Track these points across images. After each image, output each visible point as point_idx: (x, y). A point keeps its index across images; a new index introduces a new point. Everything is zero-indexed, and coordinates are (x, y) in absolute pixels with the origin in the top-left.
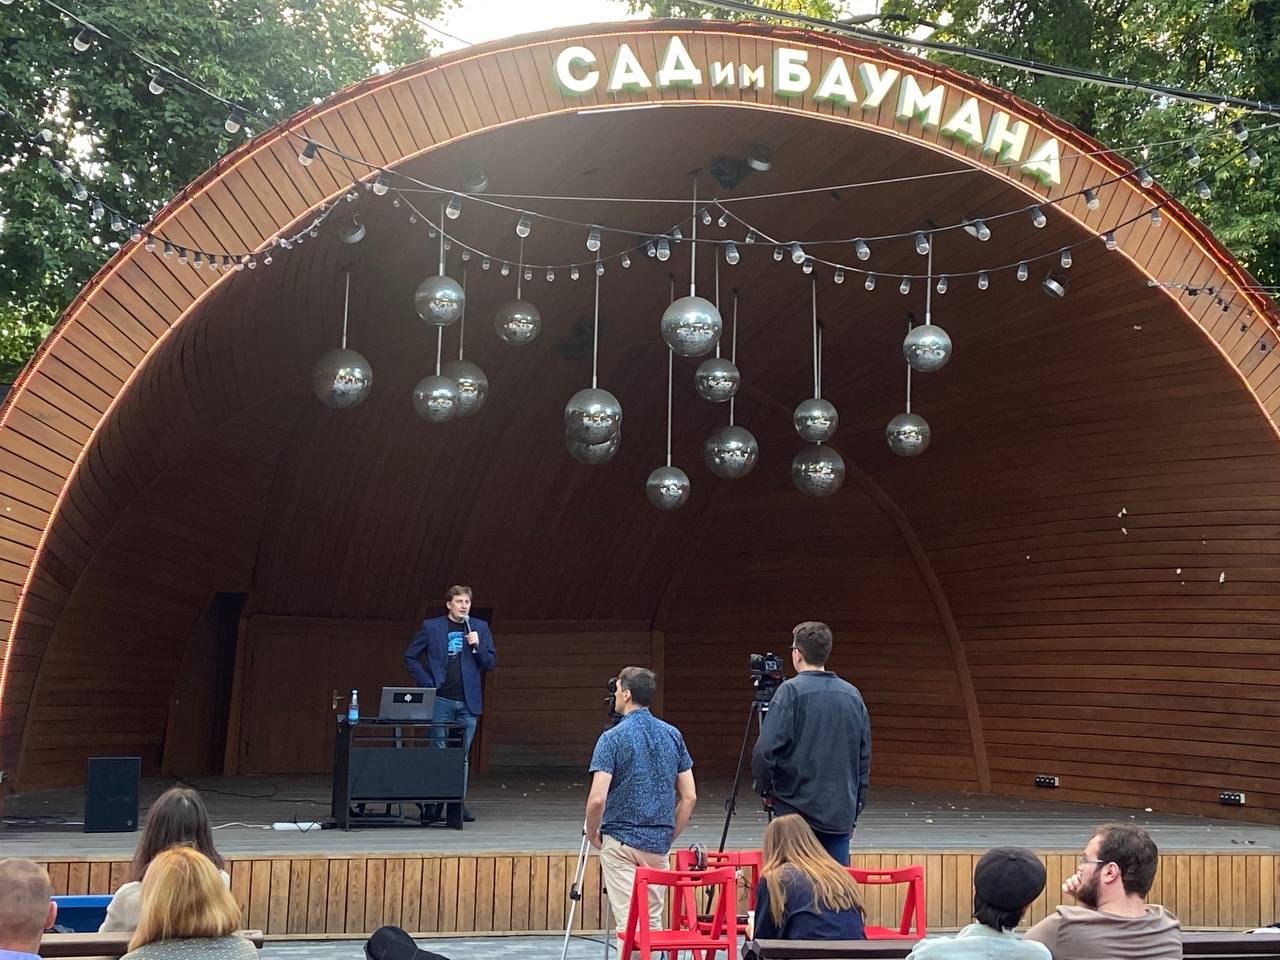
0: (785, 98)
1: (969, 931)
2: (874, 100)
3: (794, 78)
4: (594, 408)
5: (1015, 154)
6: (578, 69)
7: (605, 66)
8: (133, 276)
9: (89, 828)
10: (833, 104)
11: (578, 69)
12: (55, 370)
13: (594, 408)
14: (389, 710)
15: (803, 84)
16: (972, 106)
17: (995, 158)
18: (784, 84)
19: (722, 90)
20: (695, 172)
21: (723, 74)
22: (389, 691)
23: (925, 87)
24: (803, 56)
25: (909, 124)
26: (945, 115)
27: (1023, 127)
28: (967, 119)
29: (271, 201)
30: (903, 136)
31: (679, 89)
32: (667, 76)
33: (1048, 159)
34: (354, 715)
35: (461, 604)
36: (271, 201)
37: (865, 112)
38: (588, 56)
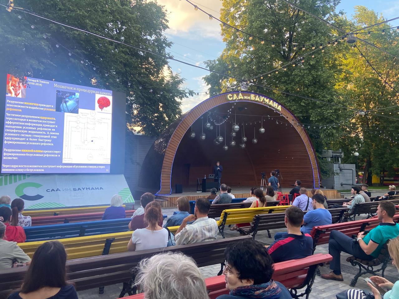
0: (252, 100)
1: (283, 288)
2: (261, 101)
3: (253, 98)
4: (236, 127)
5: (276, 107)
6: (230, 97)
7: (233, 97)
8: (177, 132)
9: (176, 193)
10: (257, 101)
11: (230, 97)
12: (172, 140)
13: (236, 127)
14: (210, 177)
15: (254, 99)
16: (272, 101)
17: (274, 108)
18: (252, 99)
19: (245, 100)
21: (246, 97)
22: (210, 175)
23: (267, 99)
24: (254, 95)
25: (265, 104)
26: (269, 102)
27: (277, 104)
28: (257, 99)
29: (173, 146)
31: (241, 99)
32: (240, 98)
33: (279, 108)
34: (205, 178)
35: (218, 164)
36: (173, 146)
37: (260, 102)
38: (231, 96)
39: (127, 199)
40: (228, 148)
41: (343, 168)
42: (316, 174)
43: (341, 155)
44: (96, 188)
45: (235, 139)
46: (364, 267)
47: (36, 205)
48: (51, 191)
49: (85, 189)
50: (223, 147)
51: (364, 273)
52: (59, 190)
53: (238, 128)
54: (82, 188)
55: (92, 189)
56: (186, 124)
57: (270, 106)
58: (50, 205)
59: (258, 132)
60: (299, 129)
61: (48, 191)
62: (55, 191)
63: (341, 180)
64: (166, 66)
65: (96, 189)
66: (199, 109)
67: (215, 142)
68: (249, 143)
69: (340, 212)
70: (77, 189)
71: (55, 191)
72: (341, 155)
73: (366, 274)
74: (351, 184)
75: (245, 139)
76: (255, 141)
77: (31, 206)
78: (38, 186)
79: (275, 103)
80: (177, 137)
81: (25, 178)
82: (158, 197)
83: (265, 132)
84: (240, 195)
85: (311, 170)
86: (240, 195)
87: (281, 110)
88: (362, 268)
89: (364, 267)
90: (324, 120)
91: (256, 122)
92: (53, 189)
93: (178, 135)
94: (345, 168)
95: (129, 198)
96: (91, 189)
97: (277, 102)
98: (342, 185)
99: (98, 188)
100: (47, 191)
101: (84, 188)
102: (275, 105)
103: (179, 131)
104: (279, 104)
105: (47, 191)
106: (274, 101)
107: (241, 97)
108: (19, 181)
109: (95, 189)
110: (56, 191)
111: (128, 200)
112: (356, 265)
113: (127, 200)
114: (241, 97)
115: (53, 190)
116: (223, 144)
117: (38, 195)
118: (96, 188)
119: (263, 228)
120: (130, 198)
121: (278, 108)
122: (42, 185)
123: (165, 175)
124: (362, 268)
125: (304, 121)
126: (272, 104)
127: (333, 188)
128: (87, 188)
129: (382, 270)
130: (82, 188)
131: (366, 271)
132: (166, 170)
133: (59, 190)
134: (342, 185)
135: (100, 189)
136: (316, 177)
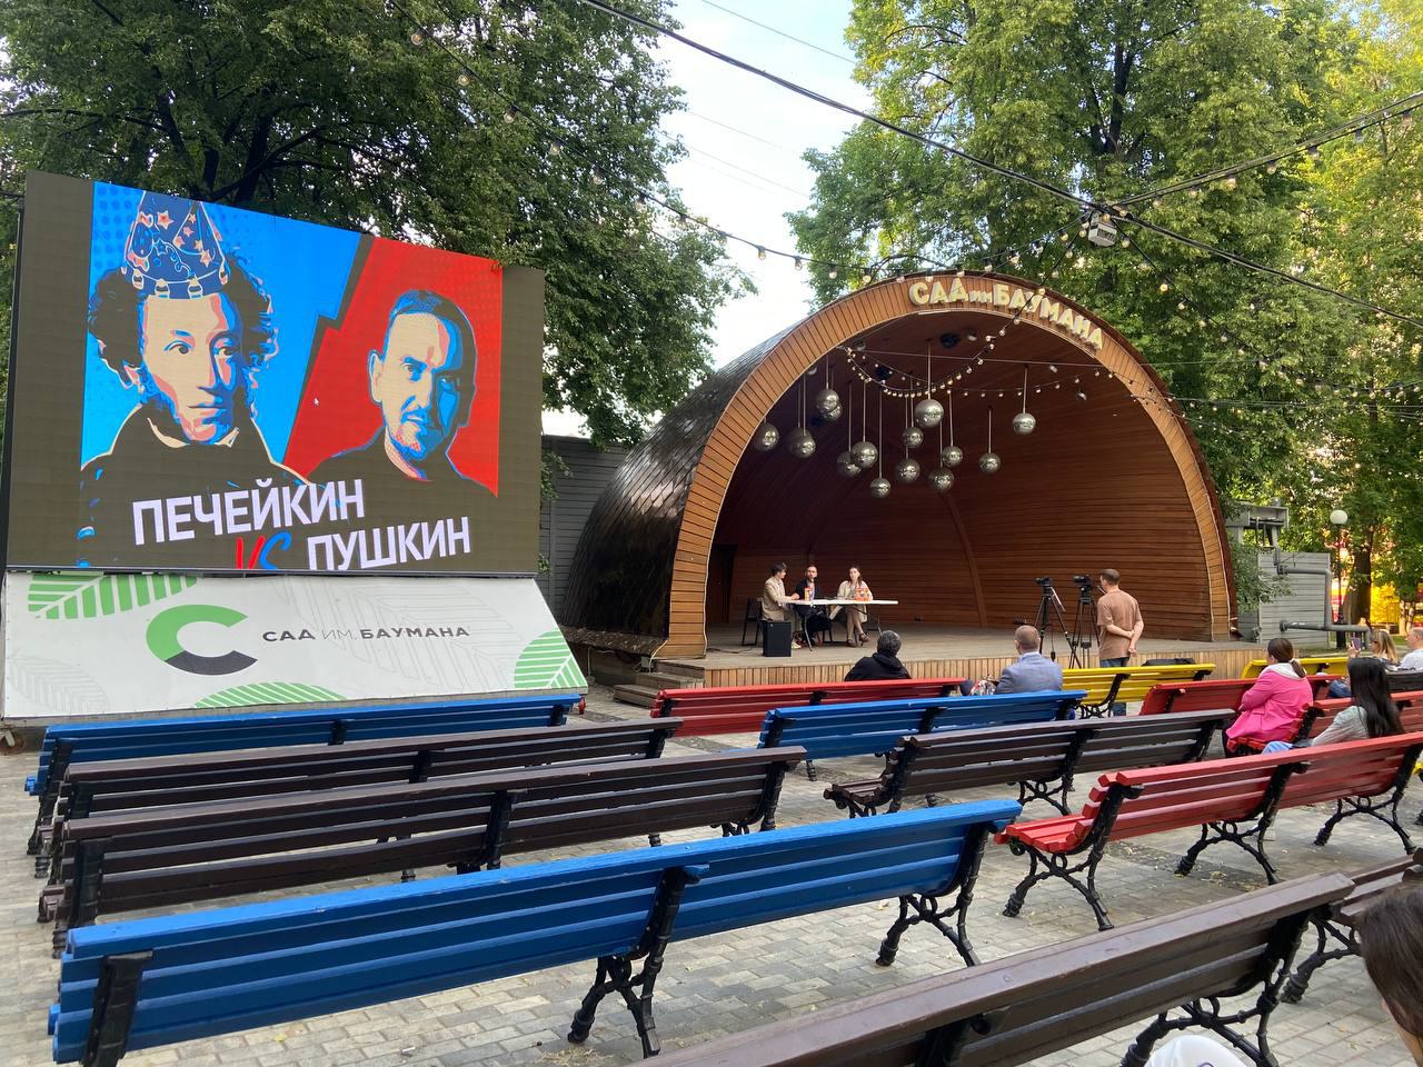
0: (997, 307)
5: (1085, 335)
6: (921, 293)
7: (930, 292)
11: (921, 293)
15: (1005, 303)
17: (1077, 337)
18: (999, 302)
20: (929, 340)
24: (1006, 288)
27: (1088, 322)
30: (1042, 326)
31: (959, 302)
32: (954, 297)
33: (1096, 337)
39: (560, 671)
40: (892, 489)
41: (1291, 567)
42: (1218, 593)
43: (1281, 518)
44: (441, 629)
45: (917, 454)
46: (1336, 933)
47: (231, 690)
48: (300, 638)
49: (404, 634)
50: (873, 485)
51: (1215, 840)
52: (310, 636)
53: (937, 413)
54: (394, 629)
55: (430, 632)
56: (760, 394)
57: (1062, 328)
58: (286, 694)
59: (1006, 428)
60: (1163, 421)
61: (269, 637)
62: (293, 638)
63: (1280, 609)
64: (999, 44)
65: (443, 633)
66: (807, 336)
67: (842, 464)
68: (968, 470)
69: (1398, 751)
70: (375, 634)
71: (293, 638)
72: (1281, 518)
73: (1344, 959)
74: (1321, 625)
75: (955, 455)
76: (992, 463)
77: (213, 697)
78: (229, 617)
79: (1081, 317)
80: (726, 442)
81: (180, 590)
82: (659, 667)
83: (1035, 431)
84: (960, 663)
85: (1198, 574)
86: (960, 663)
87: (1100, 346)
88: (1327, 933)
89: (1336, 933)
90: (1254, 387)
91: (1060, 384)
92: (288, 633)
93: (730, 435)
94: (1298, 567)
95: (565, 670)
96: (424, 633)
97: (1087, 316)
98: (1282, 630)
99: (450, 631)
100: (265, 636)
101: (400, 630)
102: (1079, 326)
103: (739, 422)
104: (1096, 323)
105: (265, 636)
106: (1077, 310)
107: (959, 292)
108: (157, 598)
109: (439, 633)
110: (300, 638)
111: (562, 674)
112: (1022, 853)
113: (559, 677)
114: (959, 292)
115: (286, 635)
116: (869, 473)
117: (234, 653)
118: (441, 629)
119: (823, 749)
120: (569, 669)
121: (1092, 339)
122: (246, 617)
123: (686, 586)
124: (1327, 933)
125: (1184, 387)
126: (1070, 323)
127: (1253, 639)
128: (409, 631)
129: (1088, 868)
130: (394, 629)
131: (1343, 947)
132: (689, 566)
133: (310, 636)
134: (1283, 628)
135: (427, 635)
136: (1219, 598)
